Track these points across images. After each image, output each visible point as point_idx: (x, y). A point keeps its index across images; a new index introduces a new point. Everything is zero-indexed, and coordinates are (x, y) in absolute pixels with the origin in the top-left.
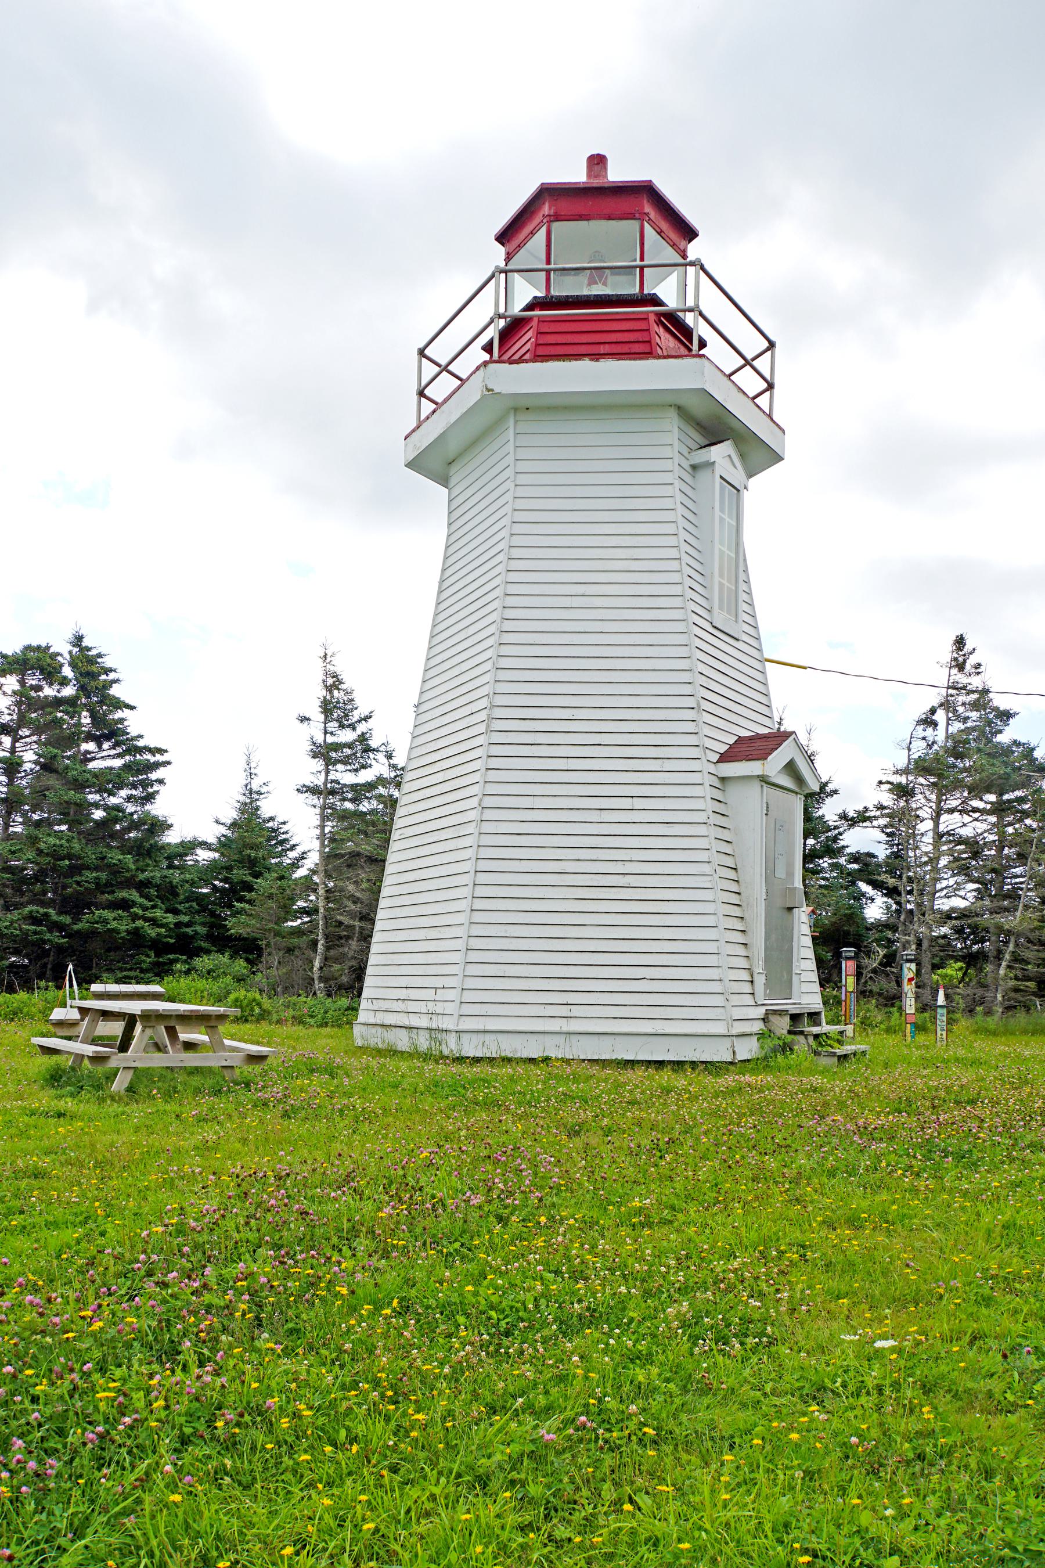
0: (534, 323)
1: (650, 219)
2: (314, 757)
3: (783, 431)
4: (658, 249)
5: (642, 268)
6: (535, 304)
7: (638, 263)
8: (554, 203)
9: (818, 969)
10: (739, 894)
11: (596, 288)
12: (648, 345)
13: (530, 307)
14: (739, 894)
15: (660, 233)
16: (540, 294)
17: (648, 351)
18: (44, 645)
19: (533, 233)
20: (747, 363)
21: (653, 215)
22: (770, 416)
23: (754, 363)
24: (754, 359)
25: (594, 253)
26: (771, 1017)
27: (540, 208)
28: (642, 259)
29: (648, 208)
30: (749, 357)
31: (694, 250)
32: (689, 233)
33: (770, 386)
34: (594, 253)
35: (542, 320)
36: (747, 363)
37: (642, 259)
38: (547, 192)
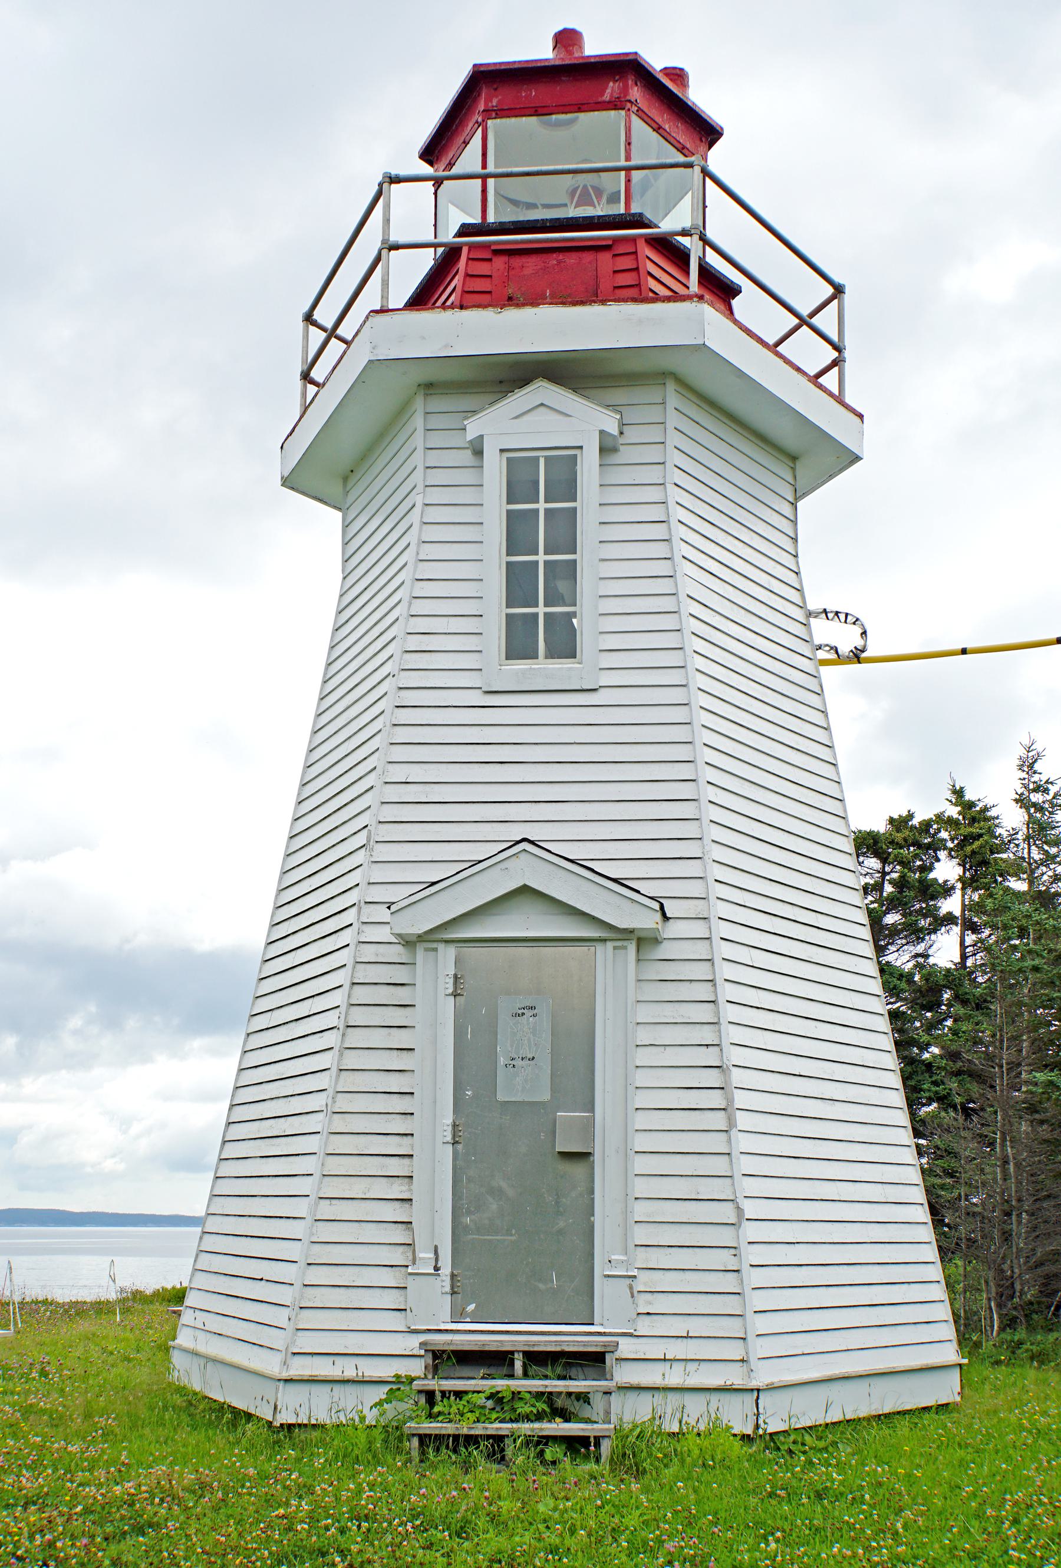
0: (465, 250)
1: (639, 109)
2: (1017, 801)
3: (861, 416)
4: (648, 144)
5: (628, 170)
6: (465, 230)
7: (623, 163)
8: (493, 89)
9: (942, 1259)
10: (744, 1339)
11: (568, 230)
12: (634, 274)
13: (461, 233)
14: (742, 1361)
15: (658, 129)
16: (476, 219)
17: (637, 293)
18: (905, 814)
19: (466, 143)
20: (803, 322)
21: (643, 104)
22: (840, 400)
23: (815, 321)
24: (812, 315)
25: (554, 162)
26: (836, 354)
27: (475, 100)
28: (628, 158)
29: (636, 93)
30: (805, 312)
31: (717, 158)
32: (708, 133)
33: (839, 290)
34: (554, 162)
35: (472, 247)
36: (803, 322)
37: (628, 158)
38: (484, 81)
